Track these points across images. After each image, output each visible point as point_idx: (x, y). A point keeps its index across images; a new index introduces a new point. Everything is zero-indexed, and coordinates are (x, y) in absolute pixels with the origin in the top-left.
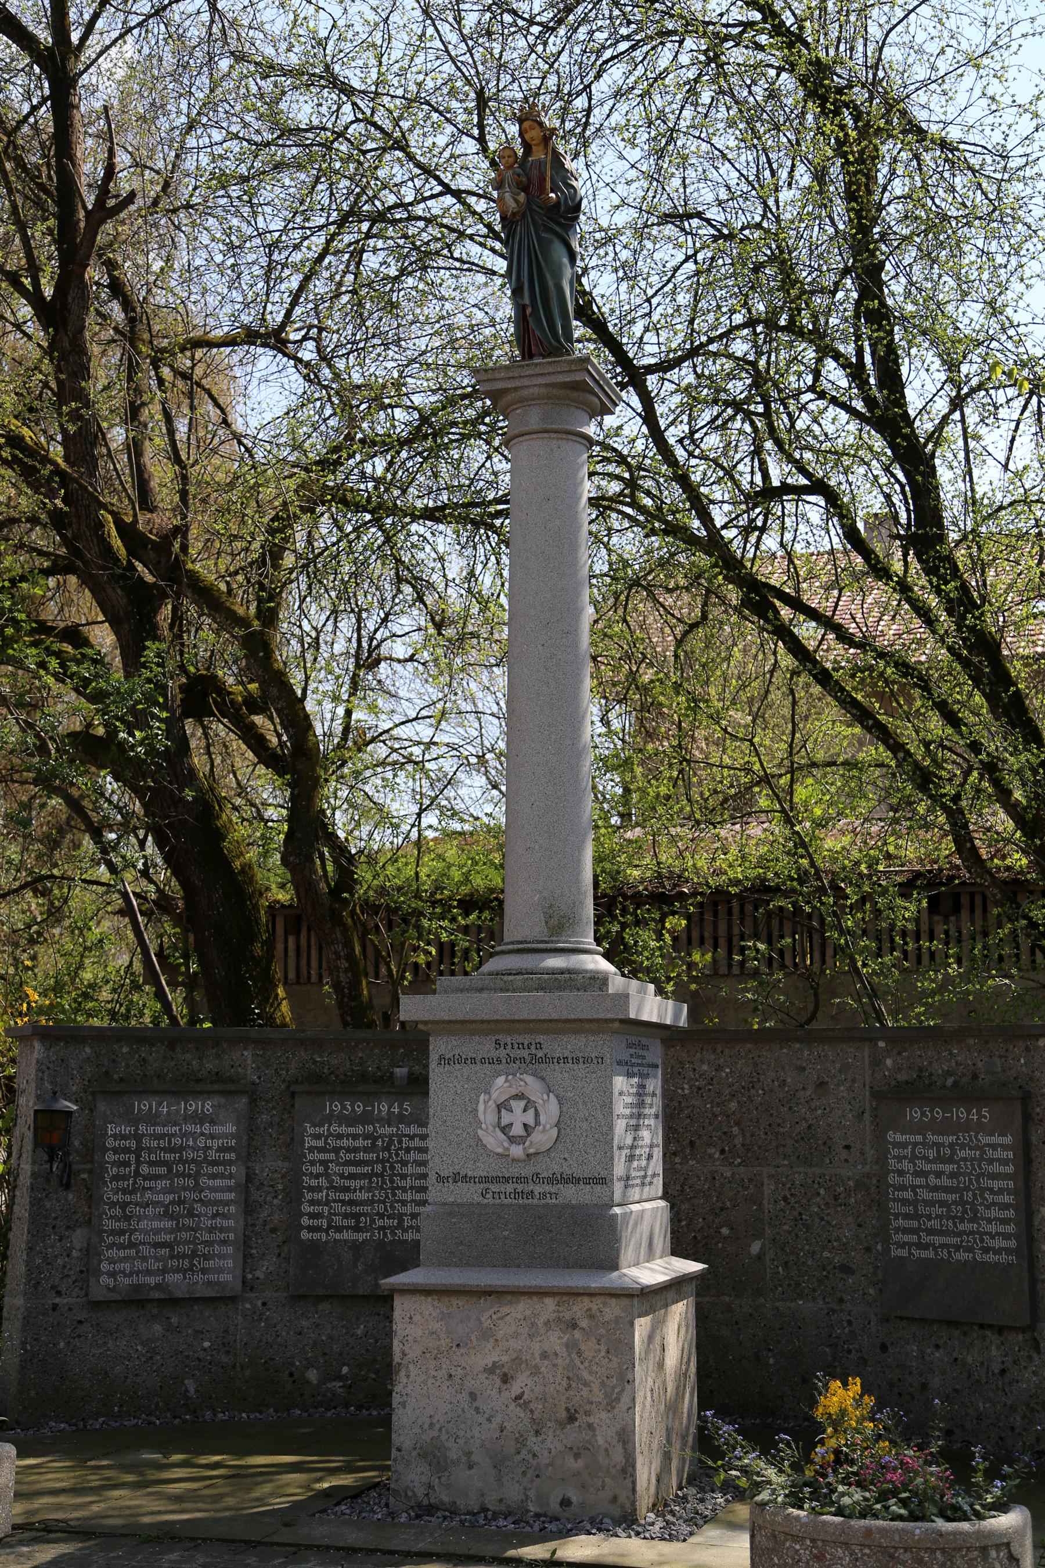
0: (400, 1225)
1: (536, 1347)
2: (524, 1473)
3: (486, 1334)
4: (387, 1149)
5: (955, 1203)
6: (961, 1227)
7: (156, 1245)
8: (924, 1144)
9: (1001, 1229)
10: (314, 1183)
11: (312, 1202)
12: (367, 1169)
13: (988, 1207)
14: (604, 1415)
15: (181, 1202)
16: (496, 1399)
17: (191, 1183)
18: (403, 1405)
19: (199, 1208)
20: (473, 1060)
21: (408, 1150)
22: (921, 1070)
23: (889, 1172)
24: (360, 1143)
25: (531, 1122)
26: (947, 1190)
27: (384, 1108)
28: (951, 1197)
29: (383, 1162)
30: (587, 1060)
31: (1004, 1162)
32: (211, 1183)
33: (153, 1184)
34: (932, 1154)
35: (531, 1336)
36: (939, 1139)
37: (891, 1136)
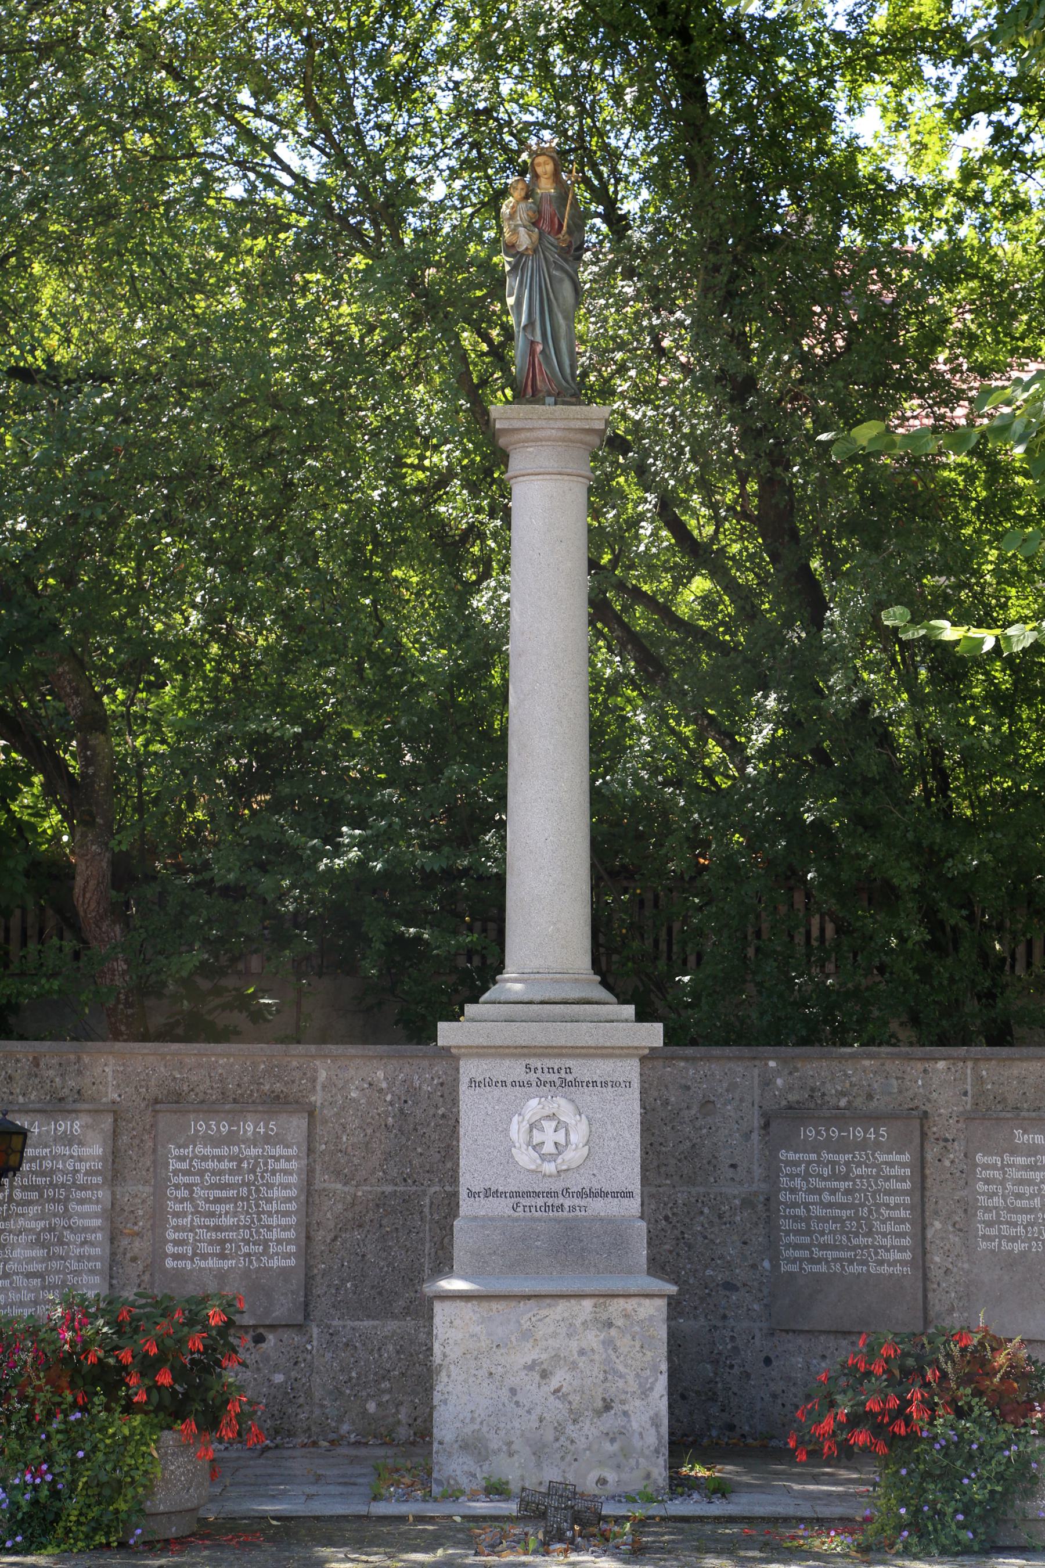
0: (266, 1252)
1: (574, 1345)
2: (563, 1458)
3: (526, 1335)
4: (253, 1171)
5: (849, 1218)
6: (855, 1242)
7: (29, 1275)
8: (819, 1162)
9: (896, 1242)
10: (178, 1208)
11: (177, 1229)
12: (232, 1193)
13: (884, 1222)
14: (638, 1403)
15: (51, 1229)
16: (535, 1393)
17: (61, 1209)
18: (445, 1402)
19: (68, 1236)
20: (504, 1083)
21: (274, 1172)
22: (813, 1090)
23: (780, 1190)
24: (226, 1165)
25: (562, 1141)
26: (842, 1206)
27: (250, 1128)
28: (845, 1213)
29: (248, 1185)
30: (615, 1084)
31: (902, 1179)
32: (79, 1208)
33: (25, 1209)
34: (826, 1172)
35: (569, 1336)
36: (836, 1157)
37: (783, 1155)
